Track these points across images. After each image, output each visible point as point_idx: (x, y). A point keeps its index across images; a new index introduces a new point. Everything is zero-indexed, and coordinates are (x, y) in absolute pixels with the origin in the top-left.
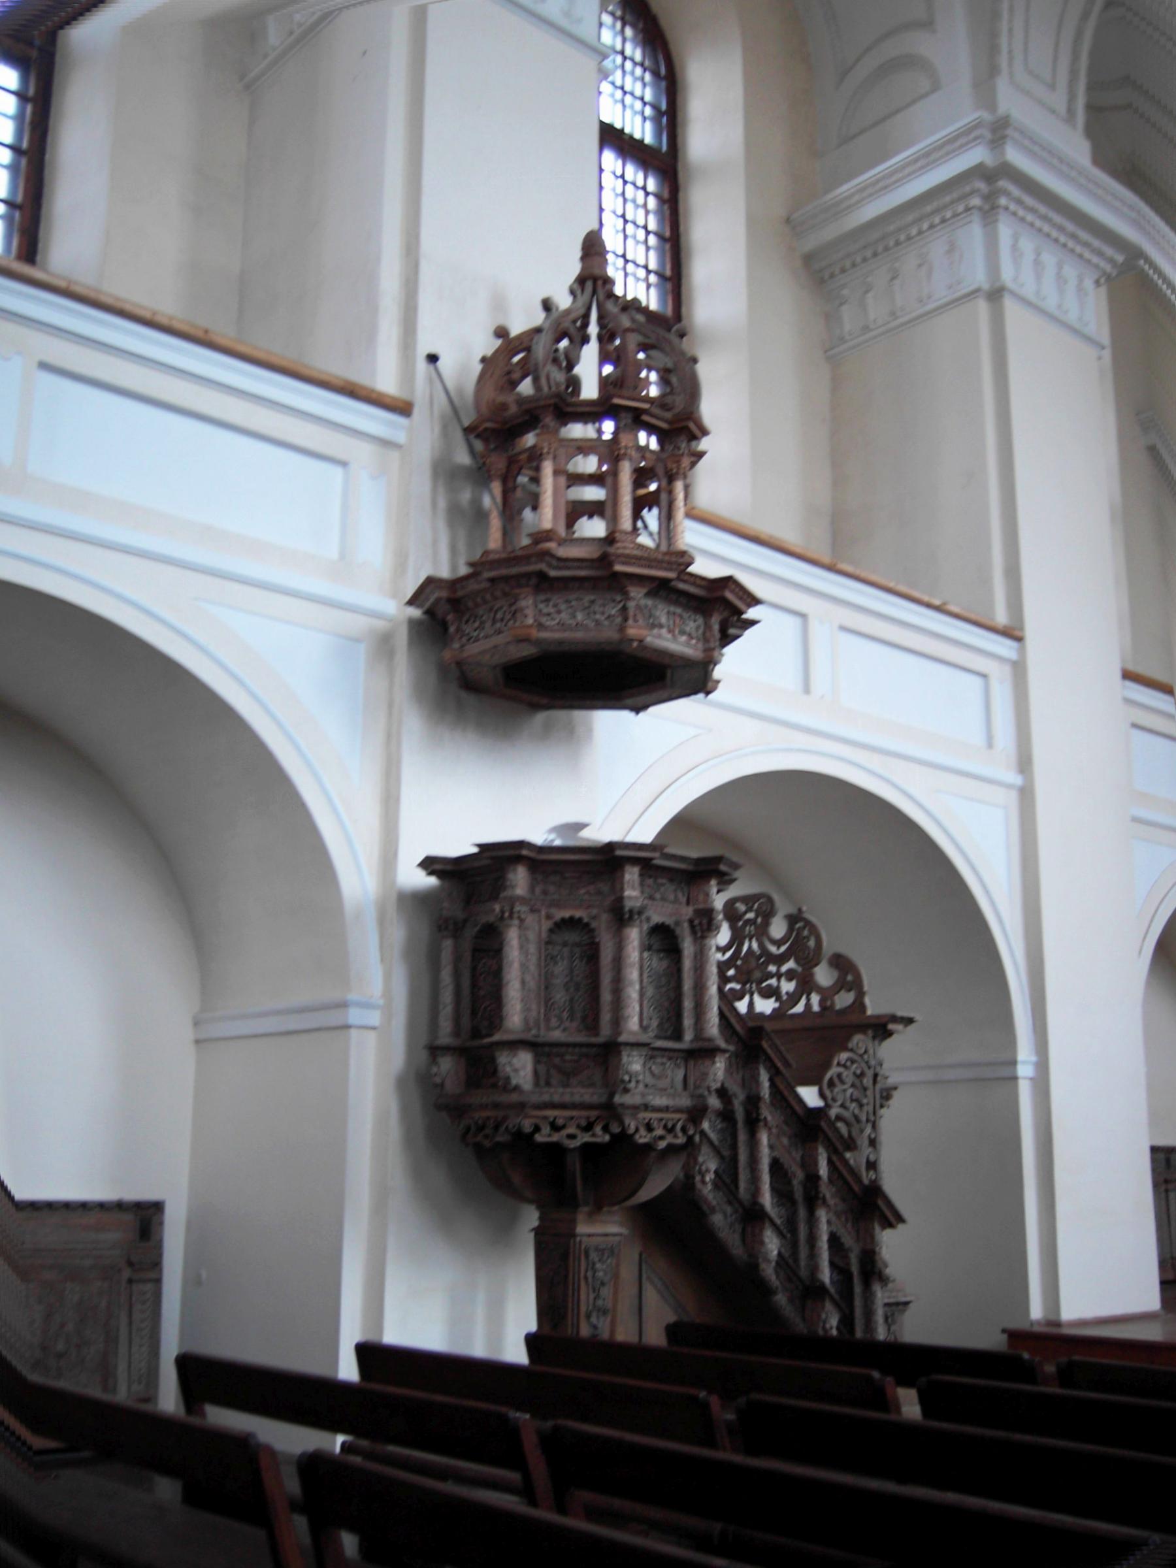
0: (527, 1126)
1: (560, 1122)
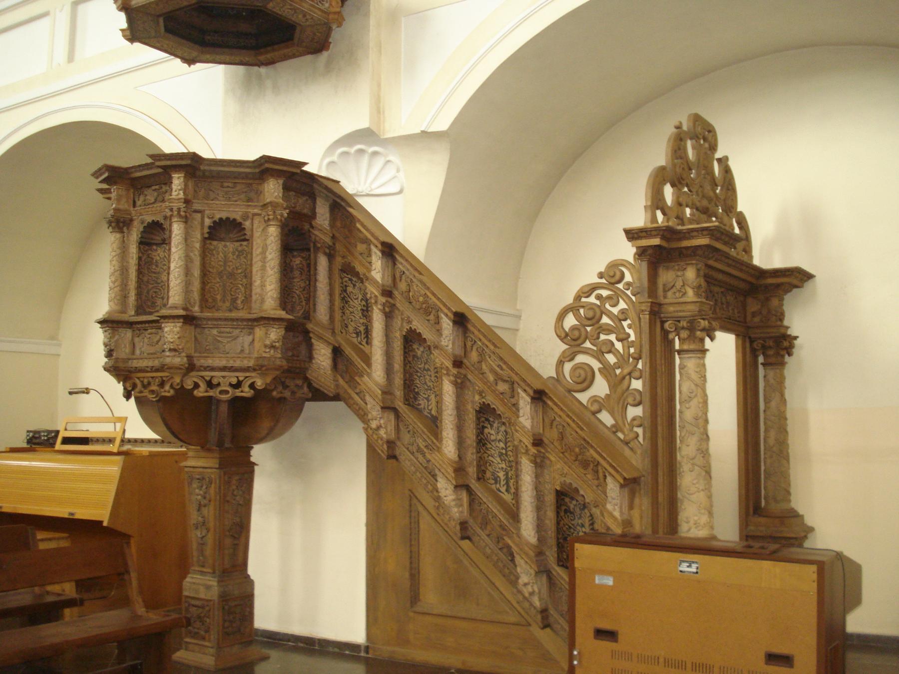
0: (189, 385)
1: (215, 381)
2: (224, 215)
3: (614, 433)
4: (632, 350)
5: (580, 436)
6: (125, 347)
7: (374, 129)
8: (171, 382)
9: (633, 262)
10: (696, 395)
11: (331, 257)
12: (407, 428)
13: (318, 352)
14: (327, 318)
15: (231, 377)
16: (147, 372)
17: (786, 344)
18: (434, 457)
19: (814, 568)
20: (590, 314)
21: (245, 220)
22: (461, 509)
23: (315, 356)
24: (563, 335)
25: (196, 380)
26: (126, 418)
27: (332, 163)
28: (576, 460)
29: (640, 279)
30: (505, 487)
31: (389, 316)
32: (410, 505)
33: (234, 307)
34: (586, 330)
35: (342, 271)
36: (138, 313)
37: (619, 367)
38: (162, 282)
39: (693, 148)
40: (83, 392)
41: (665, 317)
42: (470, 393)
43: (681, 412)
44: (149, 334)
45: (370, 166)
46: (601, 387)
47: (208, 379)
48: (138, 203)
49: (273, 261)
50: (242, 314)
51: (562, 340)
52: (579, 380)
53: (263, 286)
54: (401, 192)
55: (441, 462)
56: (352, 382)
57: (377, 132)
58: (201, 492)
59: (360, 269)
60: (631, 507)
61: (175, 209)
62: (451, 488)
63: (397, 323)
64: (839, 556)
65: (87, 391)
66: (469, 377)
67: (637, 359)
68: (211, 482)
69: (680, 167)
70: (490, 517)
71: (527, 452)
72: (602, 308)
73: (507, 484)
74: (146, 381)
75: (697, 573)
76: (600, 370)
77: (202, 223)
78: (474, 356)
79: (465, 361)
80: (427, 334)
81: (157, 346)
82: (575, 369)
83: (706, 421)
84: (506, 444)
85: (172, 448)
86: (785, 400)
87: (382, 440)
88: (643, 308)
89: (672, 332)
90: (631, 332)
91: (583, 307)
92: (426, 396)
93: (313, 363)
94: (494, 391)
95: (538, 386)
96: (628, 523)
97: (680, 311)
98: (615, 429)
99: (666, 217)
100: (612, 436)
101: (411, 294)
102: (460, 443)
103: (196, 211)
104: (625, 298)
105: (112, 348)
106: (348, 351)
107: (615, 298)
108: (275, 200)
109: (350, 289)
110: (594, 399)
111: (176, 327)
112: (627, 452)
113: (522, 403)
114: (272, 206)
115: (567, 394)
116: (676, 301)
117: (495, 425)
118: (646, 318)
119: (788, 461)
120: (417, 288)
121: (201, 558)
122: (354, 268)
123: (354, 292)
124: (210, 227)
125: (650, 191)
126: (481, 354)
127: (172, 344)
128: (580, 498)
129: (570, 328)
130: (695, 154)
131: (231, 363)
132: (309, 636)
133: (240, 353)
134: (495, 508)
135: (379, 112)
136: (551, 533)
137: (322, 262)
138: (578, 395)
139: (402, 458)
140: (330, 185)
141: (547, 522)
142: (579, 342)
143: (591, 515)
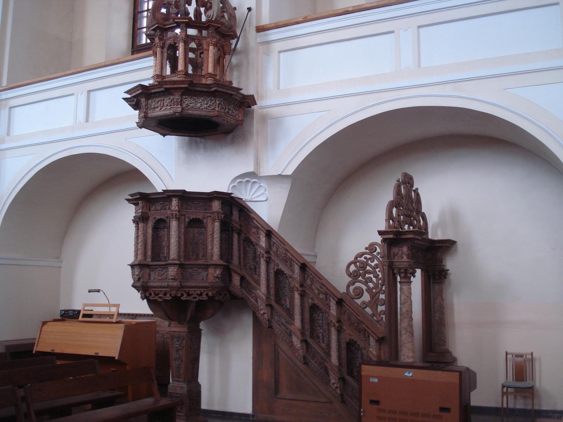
1: (191, 293)
2: (194, 217)
3: (372, 317)
4: (380, 282)
5: (358, 319)
6: (146, 276)
7: (256, 172)
8: (170, 292)
9: (381, 244)
10: (407, 302)
11: (239, 234)
12: (276, 314)
13: (234, 278)
14: (238, 262)
15: (198, 291)
16: (158, 288)
17: (444, 273)
18: (292, 328)
19: (458, 373)
20: (362, 265)
21: (204, 219)
22: (303, 350)
23: (233, 280)
24: (350, 274)
25: (182, 292)
26: (119, 305)
27: (234, 186)
28: (355, 329)
29: (384, 251)
30: (322, 340)
31: (268, 262)
32: (275, 349)
33: (197, 258)
34: (360, 272)
35: (244, 240)
36: (152, 261)
37: (374, 289)
38: (163, 246)
39: (404, 188)
40: (97, 292)
41: (394, 268)
42: (307, 299)
43: (401, 308)
44: (158, 271)
45: (252, 187)
46: (366, 297)
47: (187, 291)
48: (152, 209)
49: (218, 238)
50: (201, 262)
51: (349, 276)
52: (356, 294)
53: (212, 249)
54: (266, 200)
55: (294, 330)
56: (250, 292)
57: (256, 173)
58: (178, 343)
59: (253, 240)
60: (380, 349)
61: (174, 215)
62: (299, 341)
63: (272, 265)
64: (468, 369)
65: (98, 291)
66: (307, 291)
67: (382, 286)
68: (184, 338)
69: (399, 199)
70: (316, 354)
71: (334, 326)
72: (367, 263)
73: (323, 339)
74: (157, 292)
75: (412, 376)
76: (366, 290)
77: (185, 220)
78: (309, 282)
79: (305, 284)
80: (286, 271)
81: (163, 276)
82: (355, 289)
83: (412, 312)
84: (322, 321)
85: (149, 320)
86: (443, 299)
87: (265, 319)
88: (385, 264)
89: (397, 274)
90: (380, 273)
91: (359, 262)
92: (285, 299)
93: (232, 284)
94: (318, 298)
95: (339, 297)
96: (379, 356)
97: (401, 265)
98: (373, 315)
99: (393, 223)
100: (371, 318)
101: (278, 253)
102: (302, 321)
103: (182, 215)
104: (377, 259)
105: (141, 277)
106: (248, 277)
107: (373, 259)
108: (218, 210)
109: (247, 248)
110: (364, 303)
111: (175, 268)
112: (378, 325)
113: (332, 304)
114: (217, 213)
115: (351, 300)
116: (399, 260)
117: (318, 312)
118: (386, 268)
119: (445, 327)
120: (281, 250)
121: (178, 374)
122: (250, 240)
123: (249, 250)
124: (188, 222)
125: (388, 212)
126: (312, 281)
127: (173, 277)
128: (357, 346)
129: (353, 271)
130: (405, 191)
131: (198, 284)
132: (223, 411)
133: (201, 280)
134: (319, 350)
135: (257, 163)
136: (344, 361)
137: (236, 236)
138: (356, 300)
139: (274, 327)
140: (238, 200)
141: (343, 356)
142: (357, 277)
143: (362, 353)
